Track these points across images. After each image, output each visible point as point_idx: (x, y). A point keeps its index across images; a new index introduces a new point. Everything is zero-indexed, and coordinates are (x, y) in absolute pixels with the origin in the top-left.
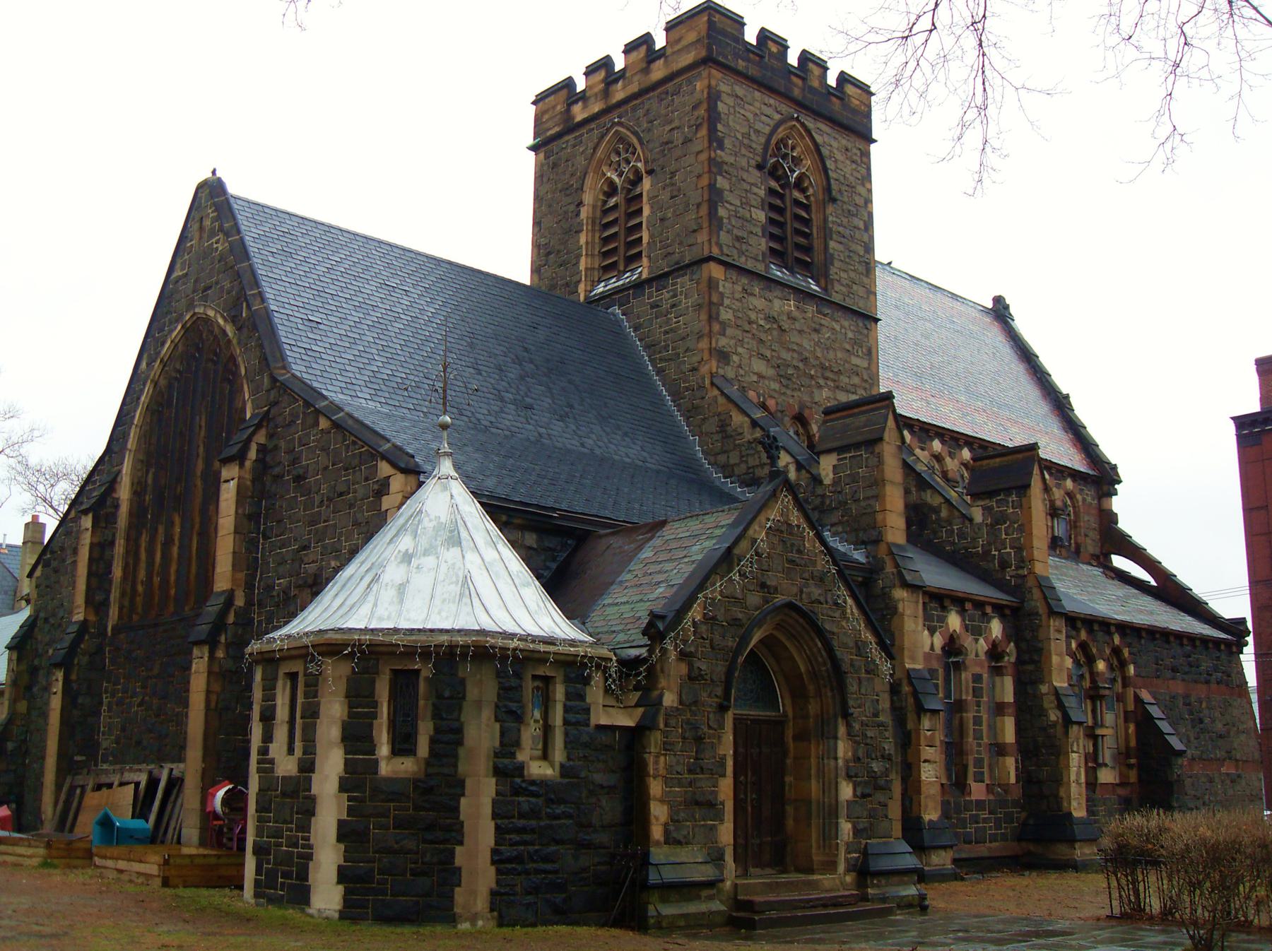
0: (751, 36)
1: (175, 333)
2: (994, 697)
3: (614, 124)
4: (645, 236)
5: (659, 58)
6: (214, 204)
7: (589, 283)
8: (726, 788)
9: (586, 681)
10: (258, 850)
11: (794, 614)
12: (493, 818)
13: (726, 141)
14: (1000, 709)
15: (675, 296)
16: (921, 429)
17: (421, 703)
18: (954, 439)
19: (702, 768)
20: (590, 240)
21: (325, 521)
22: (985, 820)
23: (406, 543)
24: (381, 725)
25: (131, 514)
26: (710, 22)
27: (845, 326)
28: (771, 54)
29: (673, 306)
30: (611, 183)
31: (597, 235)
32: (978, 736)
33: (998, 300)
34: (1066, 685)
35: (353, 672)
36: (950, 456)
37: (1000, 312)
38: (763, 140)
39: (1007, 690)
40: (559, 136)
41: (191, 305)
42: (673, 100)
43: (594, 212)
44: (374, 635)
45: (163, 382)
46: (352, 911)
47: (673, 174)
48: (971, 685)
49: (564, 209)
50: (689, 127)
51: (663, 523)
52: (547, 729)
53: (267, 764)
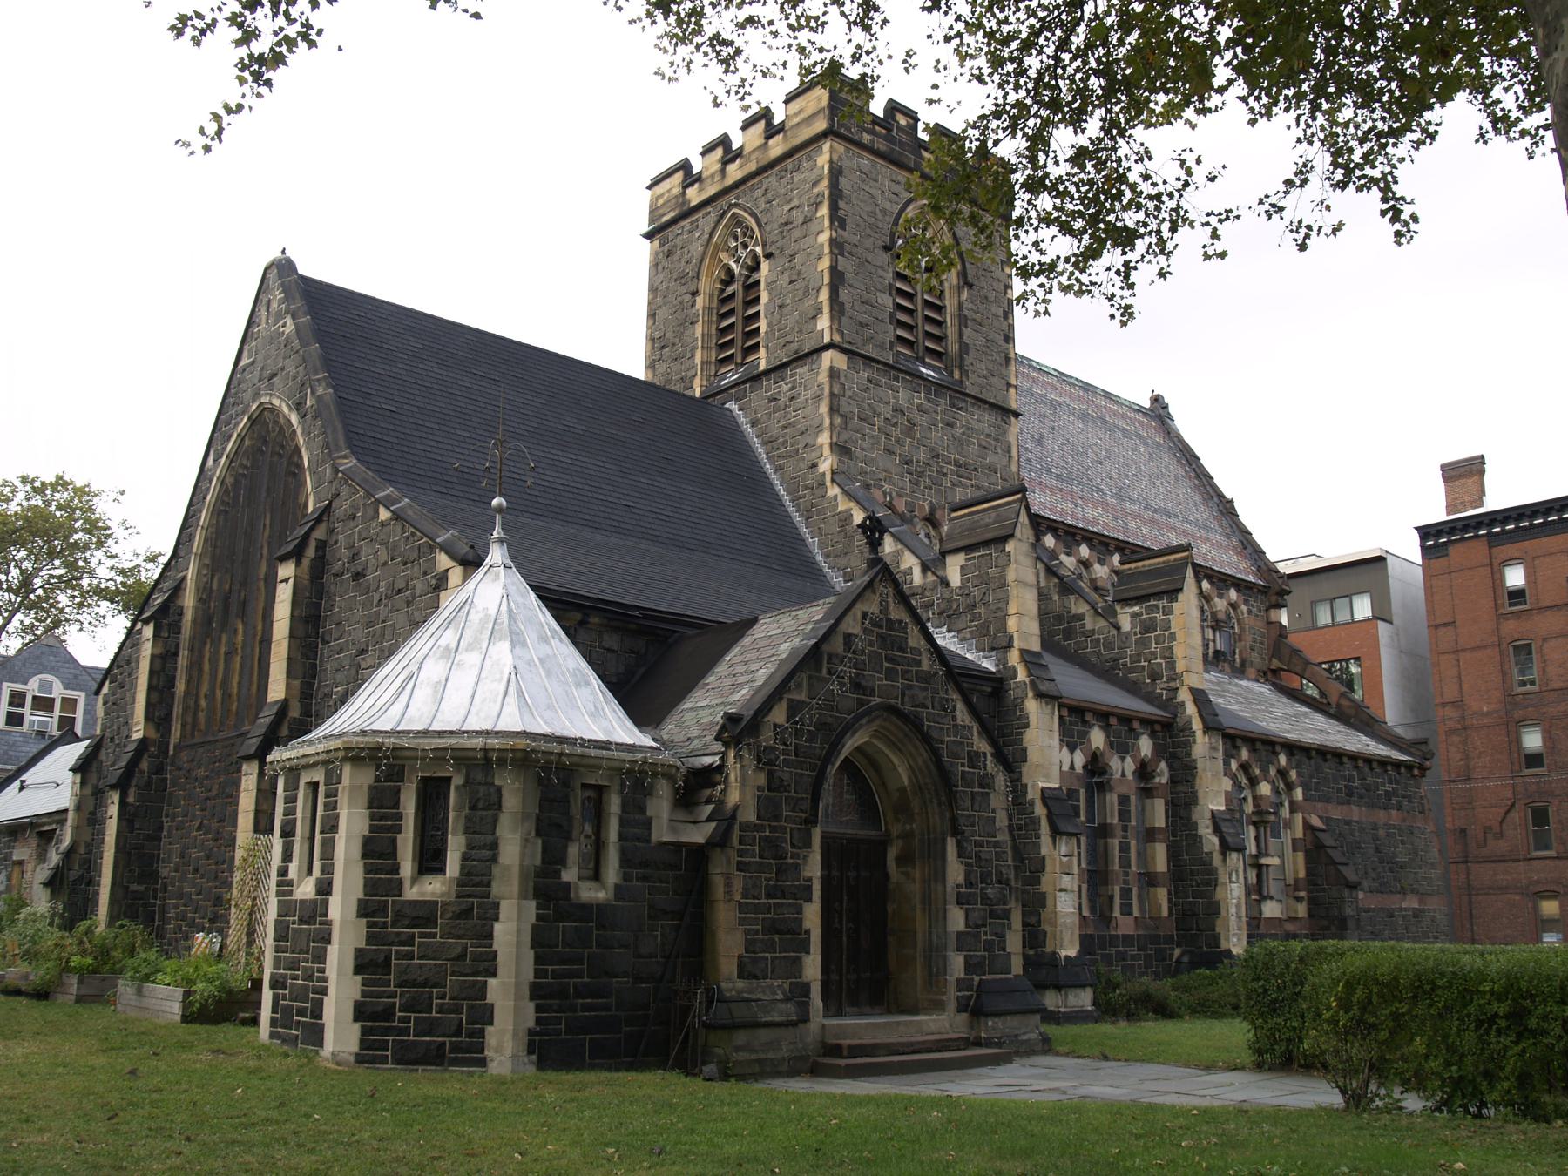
0: (877, 108)
1: (241, 426)
2: (1143, 822)
3: (731, 206)
4: (763, 325)
5: (778, 132)
6: (283, 285)
8: (812, 915)
9: (649, 792)
10: (275, 985)
11: (894, 719)
12: (532, 947)
13: (848, 221)
14: (1150, 835)
16: (1067, 533)
17: (452, 815)
18: (1103, 544)
19: (783, 892)
21: (383, 622)
22: (1133, 958)
23: (449, 637)
24: (406, 839)
25: (195, 622)
27: (985, 419)
28: (899, 128)
29: (792, 398)
30: (729, 271)
31: (714, 326)
32: (1125, 864)
33: (1157, 399)
34: (1223, 808)
35: (377, 779)
36: (1099, 562)
37: (1158, 411)
39: (1158, 814)
40: (674, 222)
41: (257, 395)
42: (792, 178)
43: (711, 301)
44: (400, 738)
45: (229, 480)
46: (369, 1053)
47: (792, 256)
48: (1116, 807)
51: (752, 622)
52: (599, 846)
53: (285, 885)
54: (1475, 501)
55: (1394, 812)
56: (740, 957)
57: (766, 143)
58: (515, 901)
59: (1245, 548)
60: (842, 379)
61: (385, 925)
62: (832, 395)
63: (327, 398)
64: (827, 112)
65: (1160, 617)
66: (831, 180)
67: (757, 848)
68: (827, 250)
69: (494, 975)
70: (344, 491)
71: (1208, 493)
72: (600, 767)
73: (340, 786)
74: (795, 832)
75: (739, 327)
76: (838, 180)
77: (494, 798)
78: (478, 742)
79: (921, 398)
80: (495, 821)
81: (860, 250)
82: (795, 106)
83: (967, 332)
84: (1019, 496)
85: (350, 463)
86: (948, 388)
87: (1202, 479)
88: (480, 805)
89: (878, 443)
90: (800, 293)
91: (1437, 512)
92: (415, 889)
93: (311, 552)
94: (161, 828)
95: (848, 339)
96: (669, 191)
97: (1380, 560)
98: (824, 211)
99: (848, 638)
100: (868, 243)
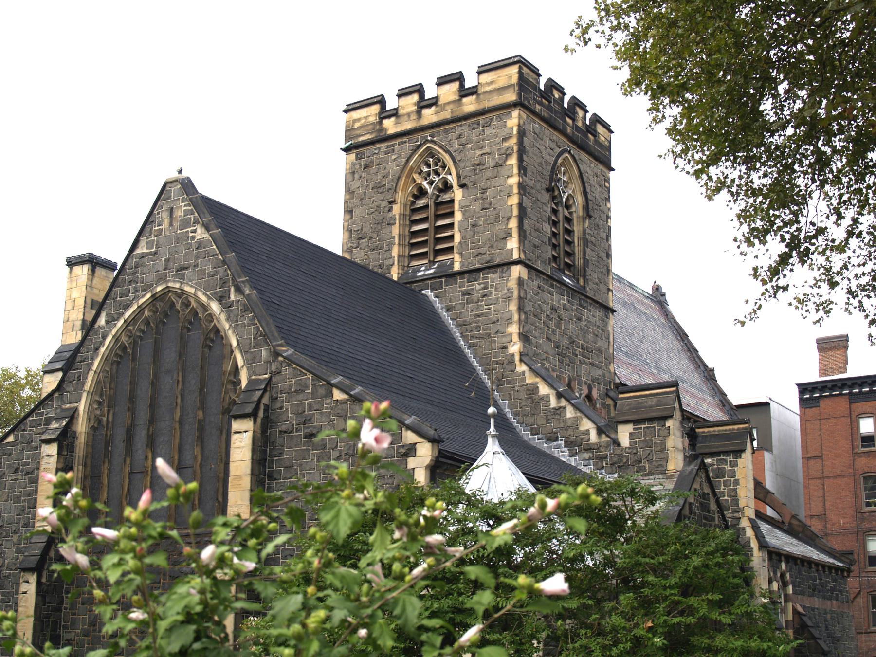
3: (427, 141)
5: (472, 94)
7: (401, 267)
13: (528, 170)
15: (485, 288)
20: (402, 233)
25: (87, 444)
26: (520, 73)
27: (598, 313)
29: (485, 296)
31: (407, 229)
33: (657, 289)
37: (658, 297)
38: (549, 168)
42: (484, 131)
43: (405, 210)
47: (484, 191)
49: (377, 204)
50: (499, 155)
54: (840, 368)
55: (834, 602)
57: (460, 100)
59: (724, 406)
60: (525, 287)
62: (520, 298)
63: (254, 296)
64: (517, 88)
65: (727, 468)
68: (515, 190)
71: (696, 363)
75: (432, 232)
79: (564, 301)
81: (534, 191)
82: (486, 78)
83: (588, 250)
84: (674, 389)
85: (288, 351)
86: (579, 293)
87: (691, 351)
89: (543, 333)
90: (492, 219)
91: (813, 376)
93: (261, 414)
94: (62, 602)
95: (528, 257)
96: (366, 118)
97: (766, 405)
98: (513, 161)
99: (690, 504)
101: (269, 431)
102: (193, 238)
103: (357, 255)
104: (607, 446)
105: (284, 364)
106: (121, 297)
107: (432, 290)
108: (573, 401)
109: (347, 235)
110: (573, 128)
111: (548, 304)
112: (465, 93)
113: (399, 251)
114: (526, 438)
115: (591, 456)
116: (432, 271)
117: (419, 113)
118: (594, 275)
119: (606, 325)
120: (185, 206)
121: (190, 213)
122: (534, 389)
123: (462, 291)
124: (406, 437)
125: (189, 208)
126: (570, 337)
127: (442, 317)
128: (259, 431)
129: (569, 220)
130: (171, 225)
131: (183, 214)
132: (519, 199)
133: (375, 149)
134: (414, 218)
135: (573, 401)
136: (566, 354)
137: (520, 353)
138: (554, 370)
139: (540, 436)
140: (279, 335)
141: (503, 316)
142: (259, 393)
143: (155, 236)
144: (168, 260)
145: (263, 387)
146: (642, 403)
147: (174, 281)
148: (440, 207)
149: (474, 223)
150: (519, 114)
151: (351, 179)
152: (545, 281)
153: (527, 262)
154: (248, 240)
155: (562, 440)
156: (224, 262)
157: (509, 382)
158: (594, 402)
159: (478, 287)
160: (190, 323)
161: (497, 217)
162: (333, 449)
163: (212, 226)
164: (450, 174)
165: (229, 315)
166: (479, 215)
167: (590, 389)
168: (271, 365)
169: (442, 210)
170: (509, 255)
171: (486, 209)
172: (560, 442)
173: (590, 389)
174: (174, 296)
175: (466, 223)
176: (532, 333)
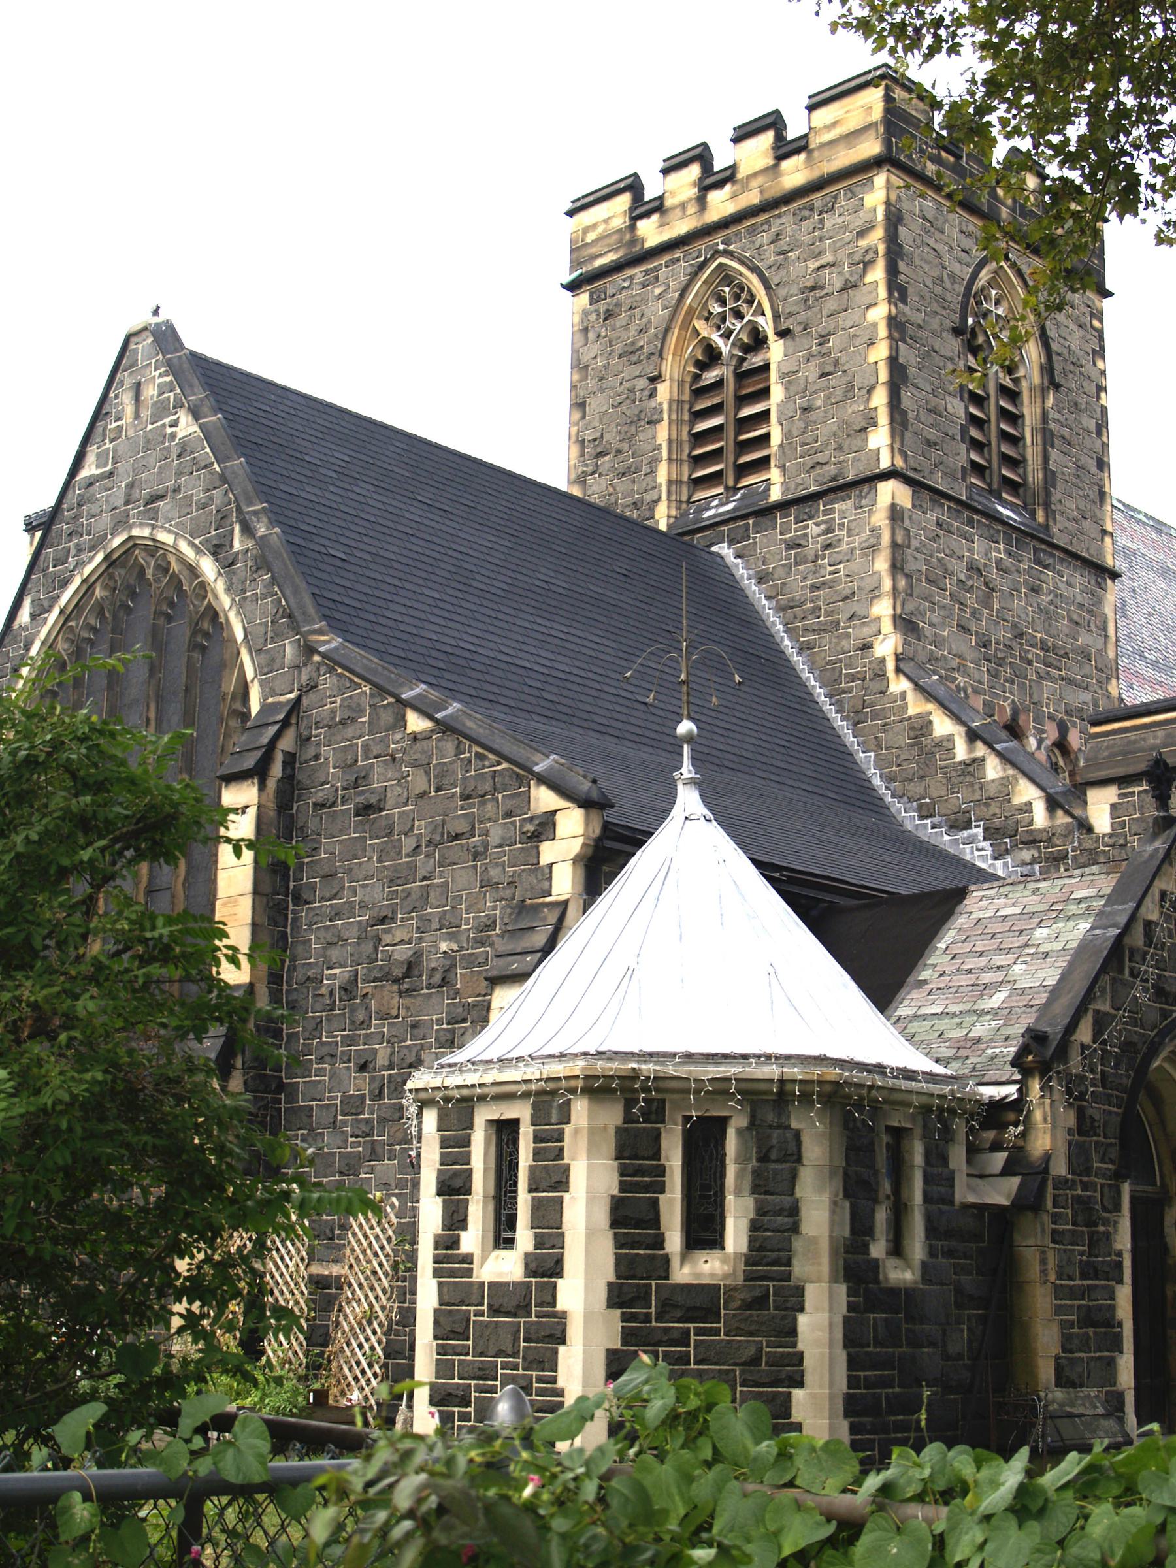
3: (717, 253)
5: (797, 151)
7: (673, 504)
12: (845, 1347)
13: (911, 291)
15: (829, 531)
19: (1096, 1271)
20: (674, 436)
21: (424, 879)
26: (888, 98)
29: (828, 546)
31: (686, 429)
35: (628, 1118)
42: (821, 221)
43: (680, 391)
47: (824, 338)
49: (627, 385)
52: (899, 1212)
56: (1057, 1358)
57: (776, 166)
58: (825, 1285)
60: (907, 523)
61: (647, 1318)
62: (894, 545)
64: (881, 129)
66: (887, 230)
67: (1069, 1211)
68: (883, 332)
69: (800, 1384)
70: (327, 682)
72: (909, 1105)
73: (568, 1129)
74: (1106, 1190)
75: (730, 431)
76: (896, 229)
77: (792, 1147)
78: (771, 1071)
79: (1000, 552)
80: (794, 1177)
81: (924, 334)
82: (823, 116)
83: (1054, 454)
85: (330, 642)
86: (1033, 537)
88: (774, 1155)
90: (839, 392)
92: (686, 1270)
93: (277, 770)
95: (912, 464)
96: (606, 221)
98: (877, 274)
99: (1148, 924)
100: (935, 323)
101: (295, 806)
102: (173, 436)
103: (594, 488)
104: (1068, 833)
105: (323, 669)
106: (54, 567)
107: (731, 542)
108: (998, 747)
109: (575, 450)
110: (1013, 210)
111: (961, 558)
112: (785, 149)
113: (669, 473)
114: (909, 826)
115: (1036, 855)
116: (730, 506)
117: (701, 201)
118: (1067, 503)
119: (1099, 601)
120: (160, 375)
121: (168, 388)
122: (922, 726)
123: (785, 541)
124: (537, 799)
125: (168, 379)
126: (1015, 626)
127: (750, 595)
128: (272, 805)
129: (1013, 395)
130: (137, 416)
131: (156, 393)
132: (891, 349)
133: (624, 280)
134: (699, 407)
135: (998, 747)
136: (1003, 659)
137: (896, 655)
138: (976, 692)
139: (936, 820)
140: (317, 612)
141: (863, 585)
142: (273, 730)
143: (111, 441)
144: (131, 486)
145: (281, 717)
146: (1135, 742)
147: (141, 525)
148: (746, 382)
149: (805, 406)
150: (888, 181)
151: (582, 342)
152: (955, 514)
153: (911, 474)
154: (298, 441)
155: (978, 826)
156: (223, 479)
157: (875, 716)
158: (1073, 756)
159: (816, 530)
160: (172, 604)
161: (850, 388)
162: (406, 834)
163: (205, 409)
164: (763, 314)
165: (230, 580)
166: (816, 387)
167: (1063, 729)
168: (300, 672)
169: (749, 386)
170: (873, 462)
171: (828, 374)
172: (974, 831)
173: (1063, 729)
174: (143, 554)
175: (791, 405)
176: (924, 616)
